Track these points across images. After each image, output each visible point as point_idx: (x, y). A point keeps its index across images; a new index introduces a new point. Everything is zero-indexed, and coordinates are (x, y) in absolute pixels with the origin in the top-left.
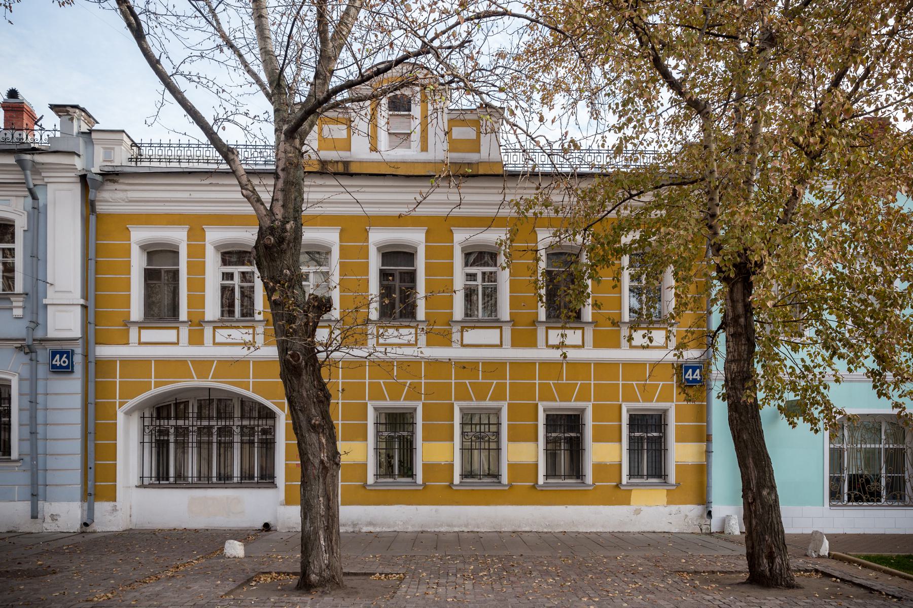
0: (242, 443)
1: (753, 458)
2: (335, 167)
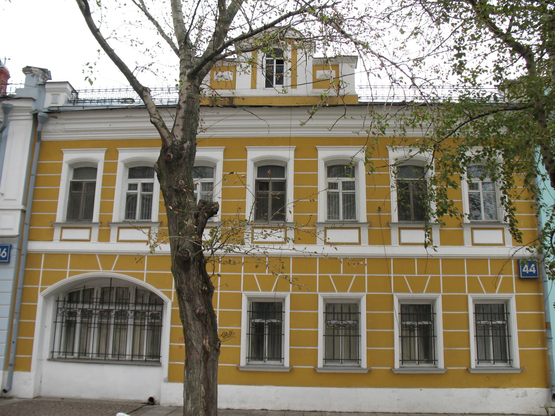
0: (135, 325)
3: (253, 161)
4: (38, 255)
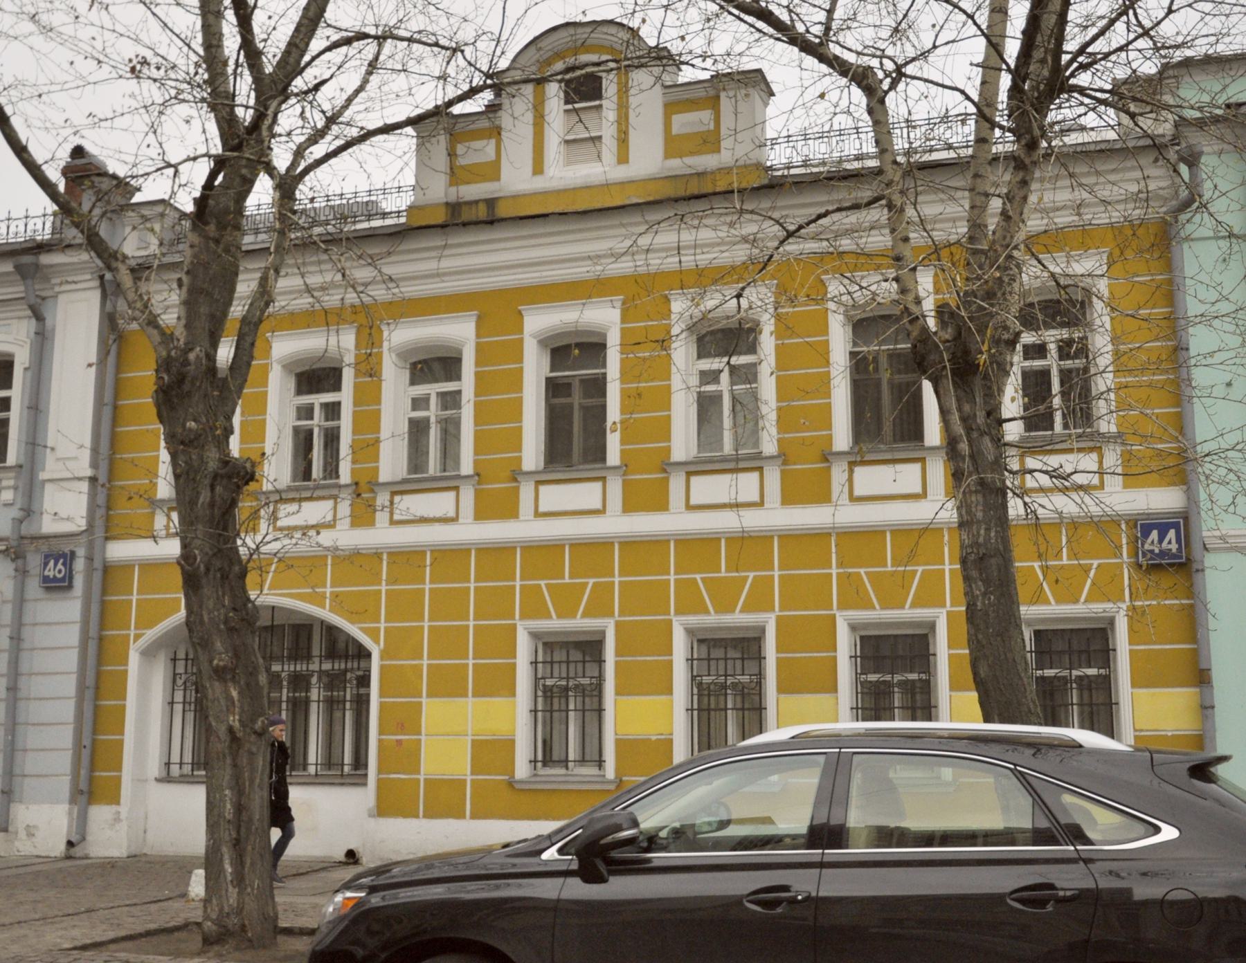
3: (535, 337)
4: (126, 567)
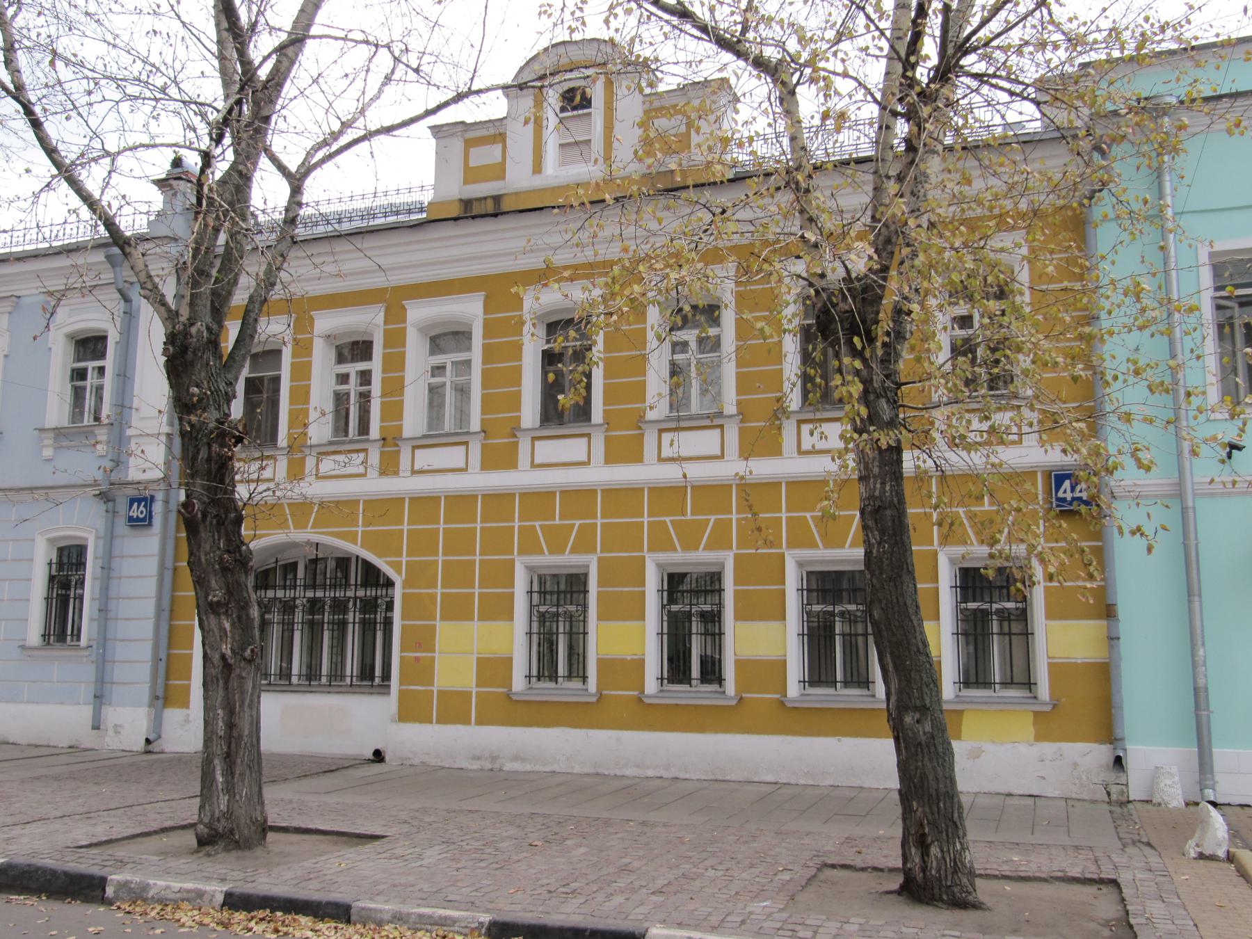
1: (892, 654)
2: (483, 205)
